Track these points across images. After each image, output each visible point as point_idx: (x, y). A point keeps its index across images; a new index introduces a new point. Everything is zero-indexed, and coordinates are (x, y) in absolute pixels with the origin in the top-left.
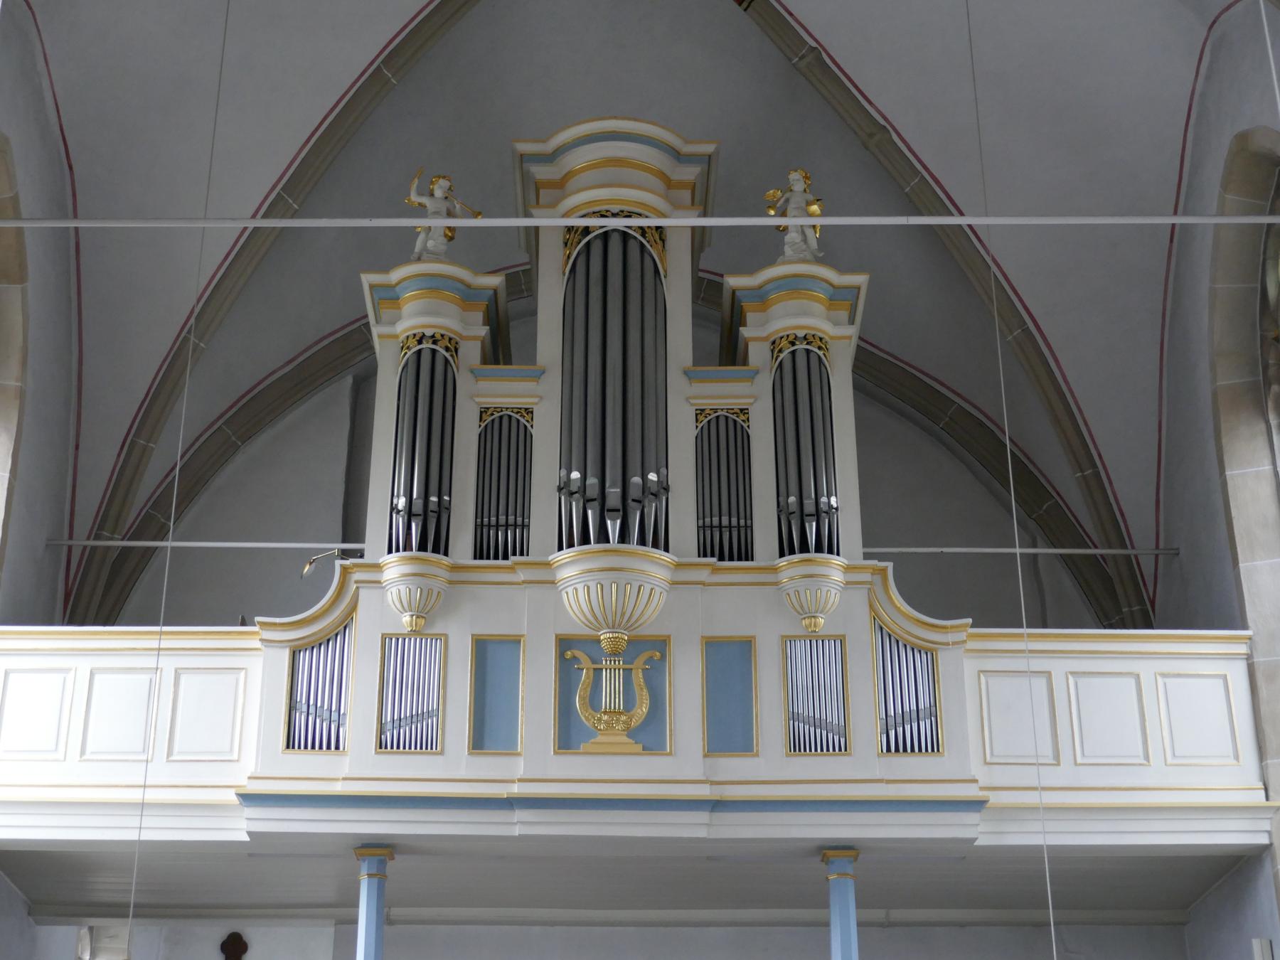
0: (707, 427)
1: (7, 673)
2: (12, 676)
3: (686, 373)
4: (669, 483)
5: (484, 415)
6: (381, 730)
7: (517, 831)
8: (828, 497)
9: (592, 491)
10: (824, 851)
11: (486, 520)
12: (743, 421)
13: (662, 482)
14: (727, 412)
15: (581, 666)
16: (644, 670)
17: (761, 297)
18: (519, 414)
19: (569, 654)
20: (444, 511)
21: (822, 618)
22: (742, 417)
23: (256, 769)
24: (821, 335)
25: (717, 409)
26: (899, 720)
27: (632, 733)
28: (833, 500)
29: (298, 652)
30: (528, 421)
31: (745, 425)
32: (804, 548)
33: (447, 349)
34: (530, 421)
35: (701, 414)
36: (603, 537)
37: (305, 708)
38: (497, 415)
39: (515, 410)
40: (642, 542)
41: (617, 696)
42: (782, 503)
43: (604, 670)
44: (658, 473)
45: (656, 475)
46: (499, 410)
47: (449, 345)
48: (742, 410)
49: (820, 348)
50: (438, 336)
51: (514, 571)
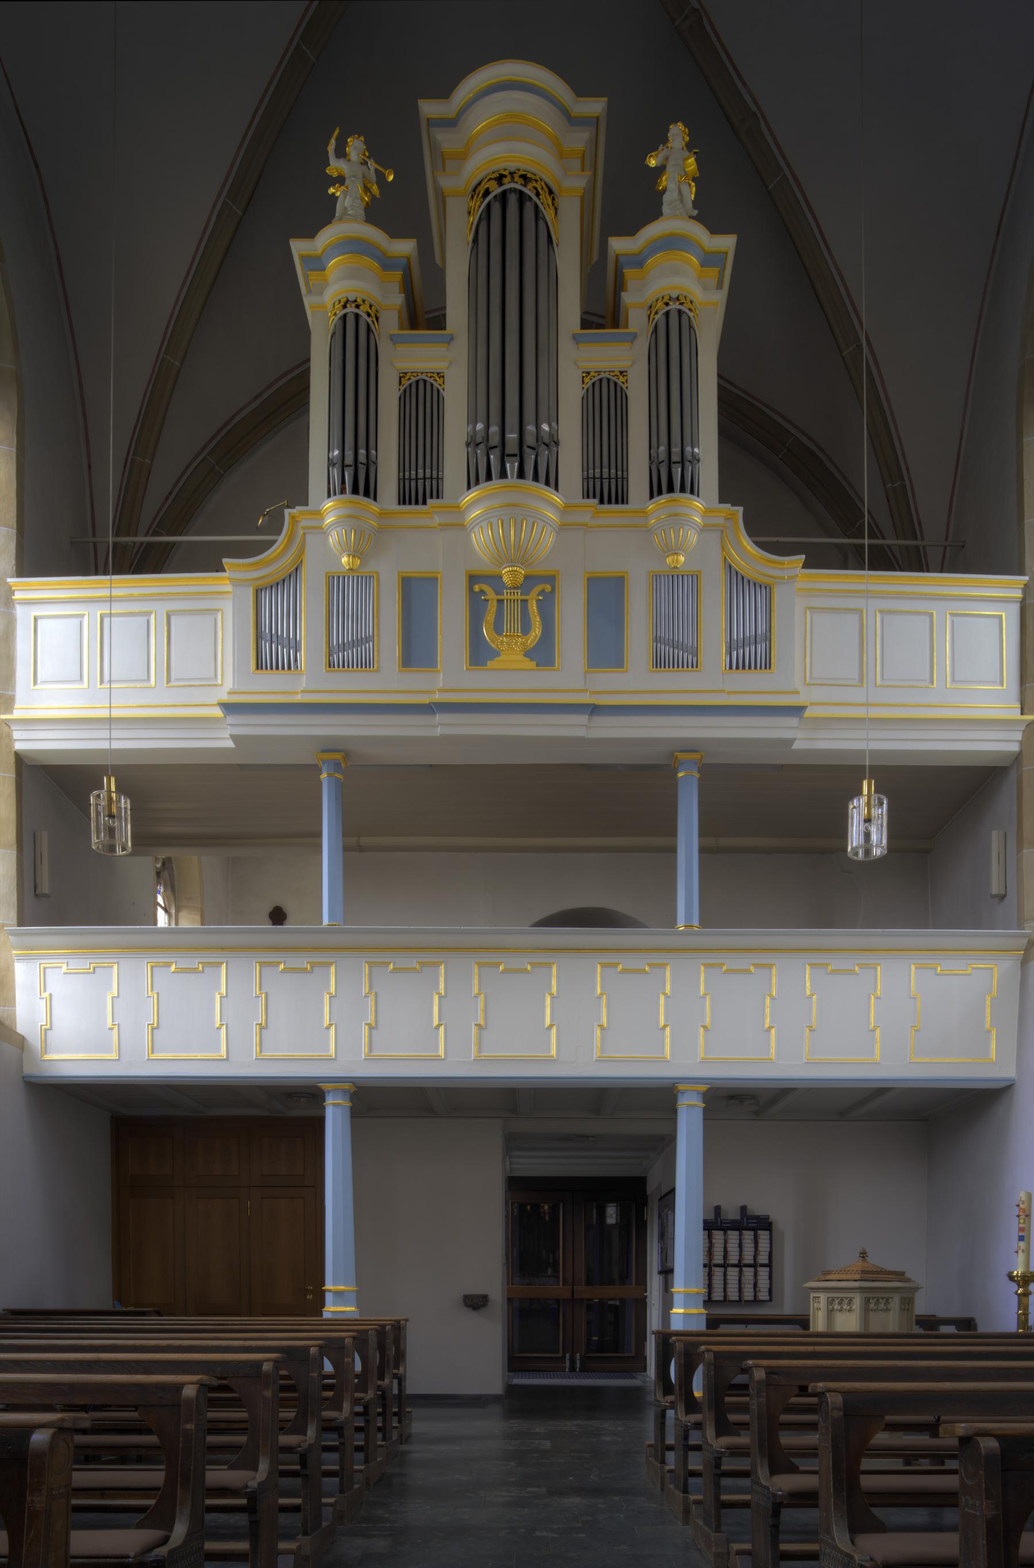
0: (592, 389)
1: (36, 619)
2: (40, 622)
3: (575, 337)
4: (559, 438)
5: (403, 379)
6: (330, 654)
7: (439, 731)
8: (692, 447)
9: (495, 440)
10: (676, 754)
11: (407, 473)
12: (623, 383)
13: (553, 435)
14: (609, 374)
15: (487, 598)
16: (538, 601)
17: (638, 261)
18: (433, 378)
19: (477, 588)
20: (371, 464)
21: (683, 555)
22: (622, 379)
23: (234, 685)
24: (692, 298)
25: (600, 372)
26: (741, 644)
27: (529, 654)
28: (696, 450)
29: (260, 590)
30: (440, 385)
31: (624, 387)
32: (671, 489)
33: (369, 315)
34: (442, 384)
35: (587, 376)
36: (503, 475)
37: (268, 638)
38: (413, 379)
39: (429, 375)
40: (536, 478)
41: (516, 622)
42: (654, 454)
43: (505, 601)
44: (550, 426)
45: (547, 426)
46: (415, 374)
47: (370, 311)
48: (621, 373)
49: (690, 310)
50: (359, 301)
51: (430, 514)
